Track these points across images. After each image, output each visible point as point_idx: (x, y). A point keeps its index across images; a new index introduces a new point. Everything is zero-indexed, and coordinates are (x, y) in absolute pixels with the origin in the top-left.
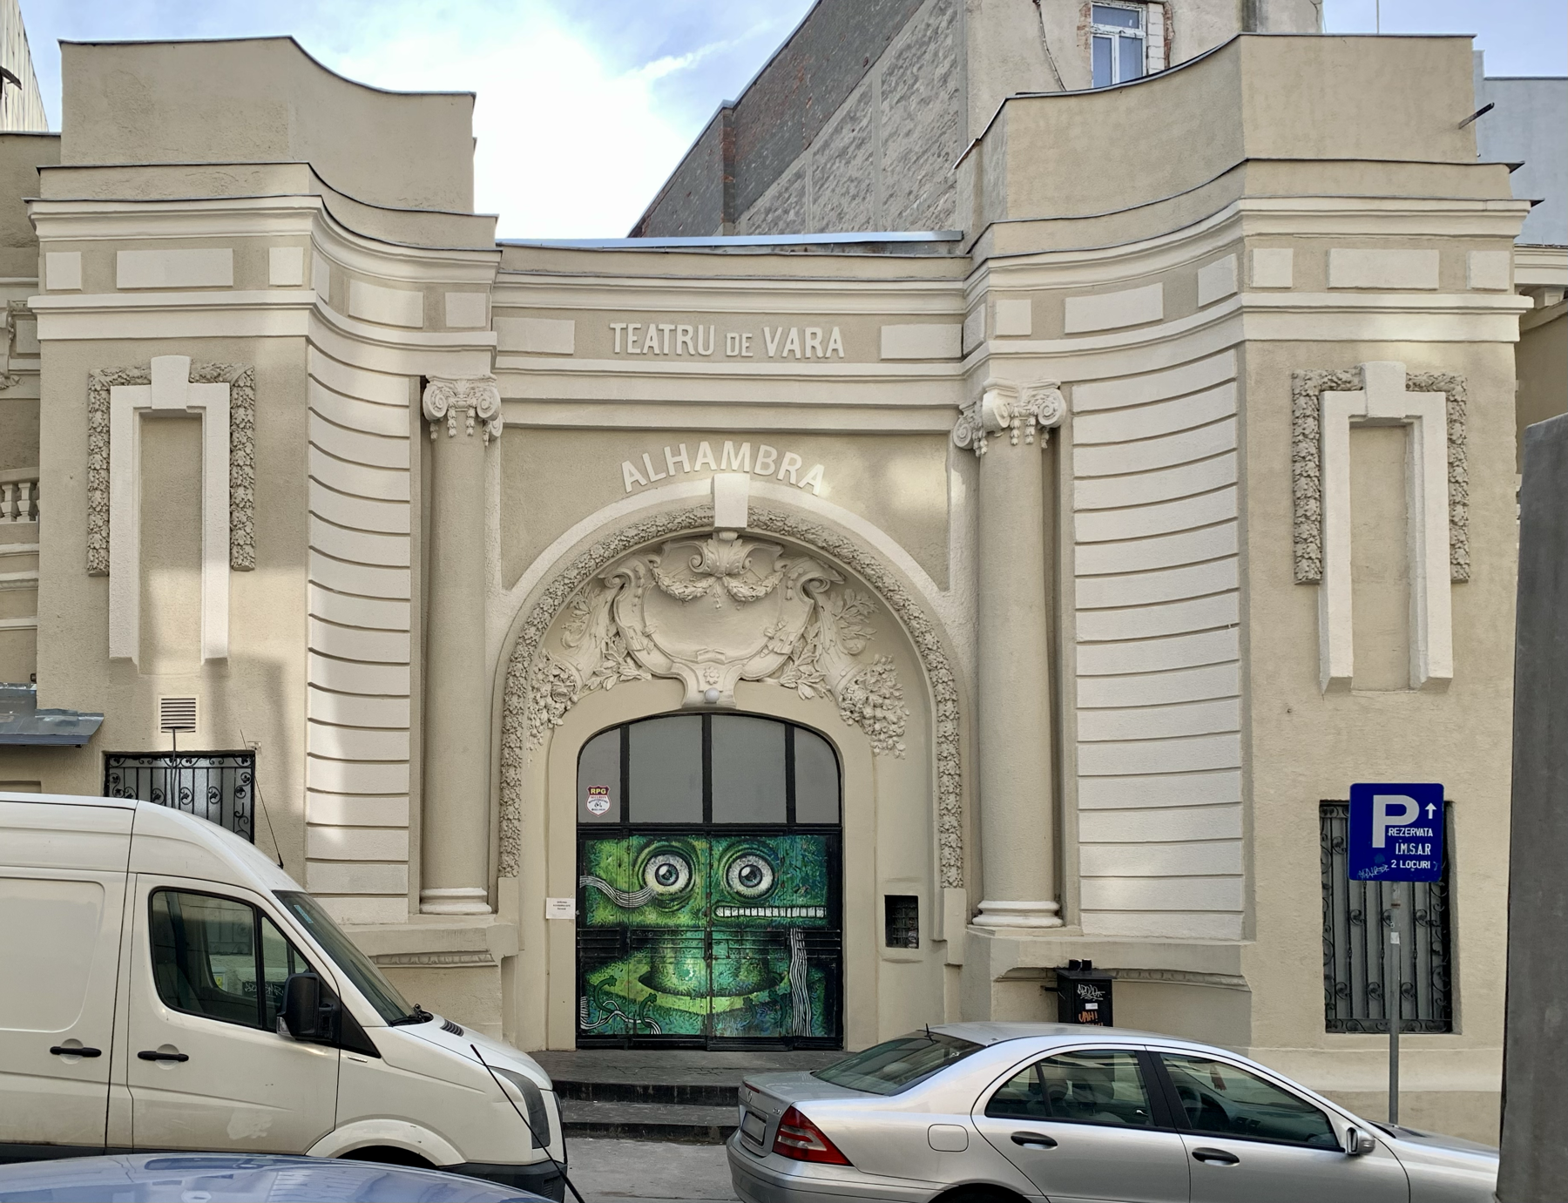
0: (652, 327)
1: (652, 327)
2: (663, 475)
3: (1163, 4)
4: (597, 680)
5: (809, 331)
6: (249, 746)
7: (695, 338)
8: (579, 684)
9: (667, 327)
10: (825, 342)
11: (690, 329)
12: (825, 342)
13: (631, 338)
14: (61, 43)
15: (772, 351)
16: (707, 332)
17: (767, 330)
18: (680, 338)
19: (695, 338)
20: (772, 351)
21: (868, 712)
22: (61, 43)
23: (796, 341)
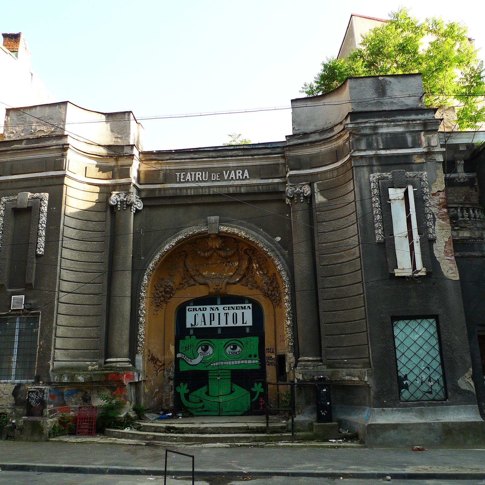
0: (189, 173)
1: (189, 173)
2: (184, 181)
3: (436, 317)
4: (181, 286)
5: (237, 172)
6: (16, 32)
7: (202, 176)
8: (174, 288)
9: (193, 173)
10: (243, 175)
11: (200, 173)
12: (243, 175)
13: (182, 177)
14: (5, 36)
15: (226, 177)
16: (205, 174)
17: (224, 172)
18: (197, 176)
19: (202, 176)
20: (226, 177)
21: (270, 292)
22: (5, 36)
23: (234, 174)
